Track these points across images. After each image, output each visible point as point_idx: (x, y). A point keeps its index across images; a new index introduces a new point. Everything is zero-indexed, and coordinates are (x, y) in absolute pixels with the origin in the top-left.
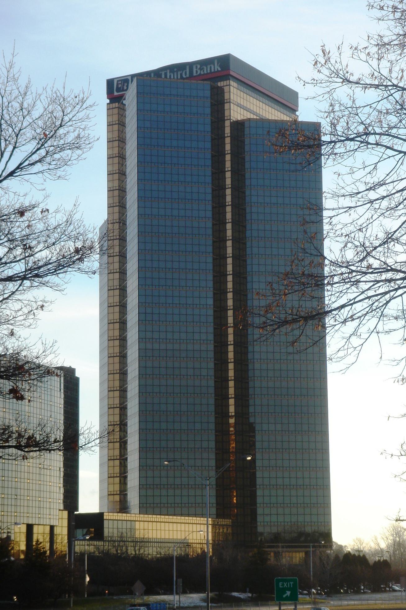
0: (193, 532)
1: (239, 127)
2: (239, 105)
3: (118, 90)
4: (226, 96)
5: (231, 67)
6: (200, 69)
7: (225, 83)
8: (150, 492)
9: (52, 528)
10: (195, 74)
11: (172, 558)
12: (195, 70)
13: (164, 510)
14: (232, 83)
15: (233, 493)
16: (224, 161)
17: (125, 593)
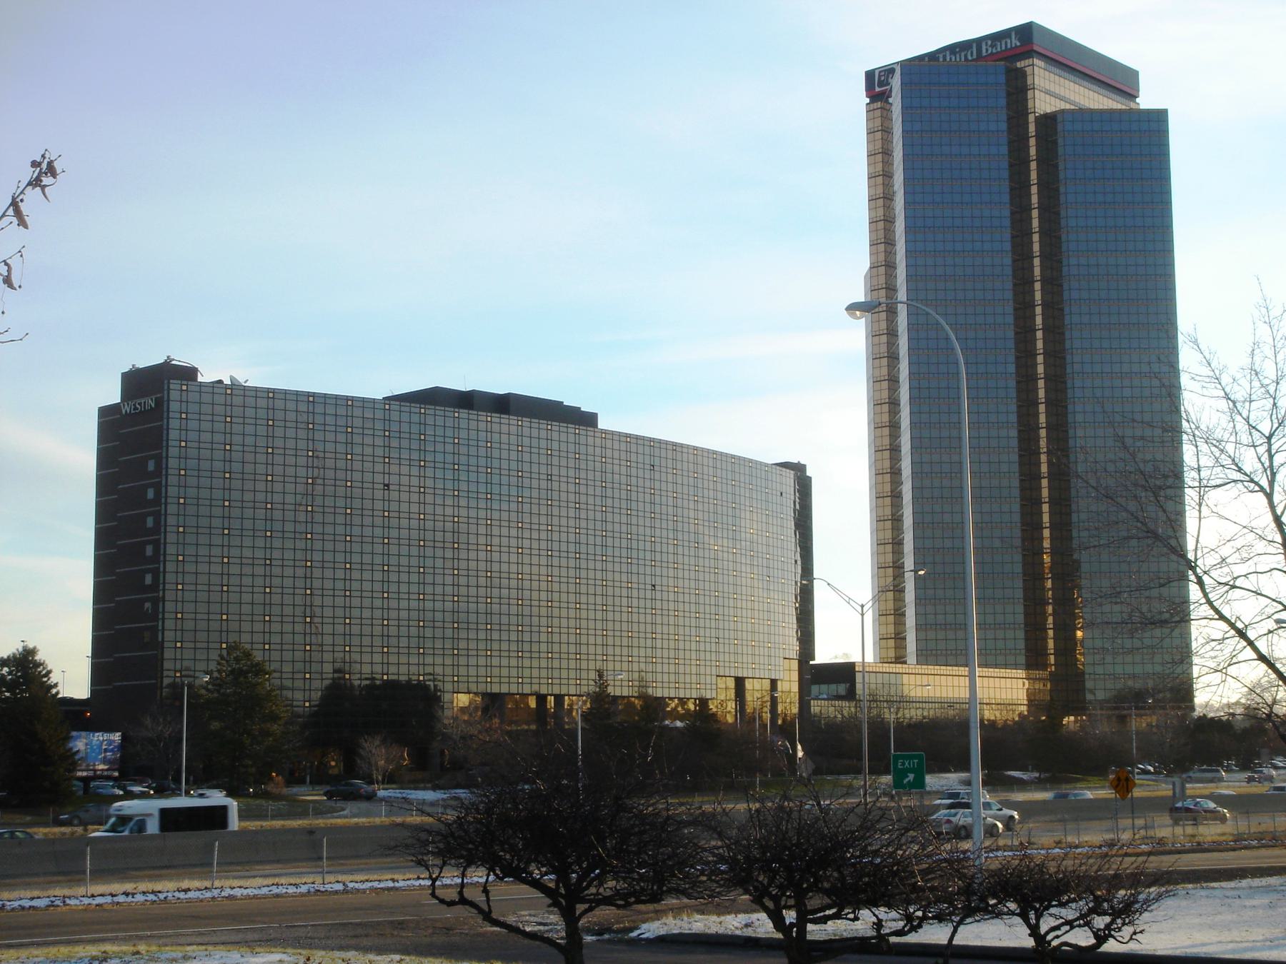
0: (1005, 691)
1: (1048, 122)
2: (1048, 92)
3: (881, 84)
4: (1029, 82)
5: (1035, 41)
6: (992, 46)
7: (1027, 62)
8: (931, 635)
9: (774, 683)
10: (984, 54)
11: (962, 726)
12: (984, 48)
13: (951, 659)
14: (1036, 61)
15: (1042, 637)
16: (1029, 171)
17: (847, 771)
